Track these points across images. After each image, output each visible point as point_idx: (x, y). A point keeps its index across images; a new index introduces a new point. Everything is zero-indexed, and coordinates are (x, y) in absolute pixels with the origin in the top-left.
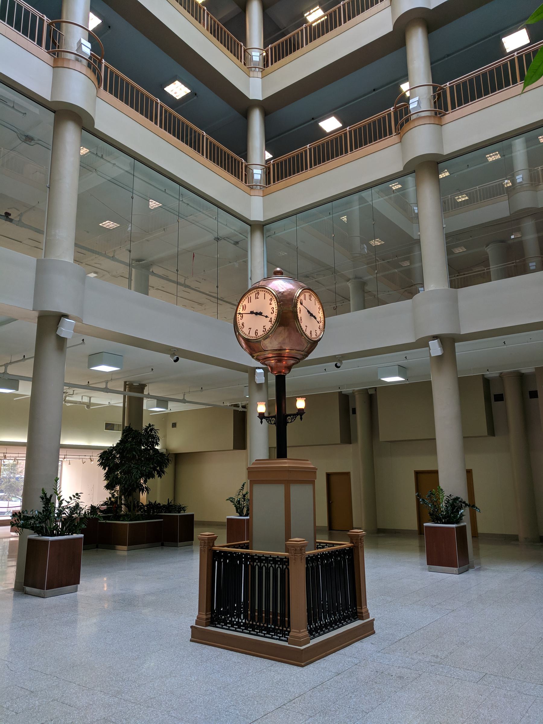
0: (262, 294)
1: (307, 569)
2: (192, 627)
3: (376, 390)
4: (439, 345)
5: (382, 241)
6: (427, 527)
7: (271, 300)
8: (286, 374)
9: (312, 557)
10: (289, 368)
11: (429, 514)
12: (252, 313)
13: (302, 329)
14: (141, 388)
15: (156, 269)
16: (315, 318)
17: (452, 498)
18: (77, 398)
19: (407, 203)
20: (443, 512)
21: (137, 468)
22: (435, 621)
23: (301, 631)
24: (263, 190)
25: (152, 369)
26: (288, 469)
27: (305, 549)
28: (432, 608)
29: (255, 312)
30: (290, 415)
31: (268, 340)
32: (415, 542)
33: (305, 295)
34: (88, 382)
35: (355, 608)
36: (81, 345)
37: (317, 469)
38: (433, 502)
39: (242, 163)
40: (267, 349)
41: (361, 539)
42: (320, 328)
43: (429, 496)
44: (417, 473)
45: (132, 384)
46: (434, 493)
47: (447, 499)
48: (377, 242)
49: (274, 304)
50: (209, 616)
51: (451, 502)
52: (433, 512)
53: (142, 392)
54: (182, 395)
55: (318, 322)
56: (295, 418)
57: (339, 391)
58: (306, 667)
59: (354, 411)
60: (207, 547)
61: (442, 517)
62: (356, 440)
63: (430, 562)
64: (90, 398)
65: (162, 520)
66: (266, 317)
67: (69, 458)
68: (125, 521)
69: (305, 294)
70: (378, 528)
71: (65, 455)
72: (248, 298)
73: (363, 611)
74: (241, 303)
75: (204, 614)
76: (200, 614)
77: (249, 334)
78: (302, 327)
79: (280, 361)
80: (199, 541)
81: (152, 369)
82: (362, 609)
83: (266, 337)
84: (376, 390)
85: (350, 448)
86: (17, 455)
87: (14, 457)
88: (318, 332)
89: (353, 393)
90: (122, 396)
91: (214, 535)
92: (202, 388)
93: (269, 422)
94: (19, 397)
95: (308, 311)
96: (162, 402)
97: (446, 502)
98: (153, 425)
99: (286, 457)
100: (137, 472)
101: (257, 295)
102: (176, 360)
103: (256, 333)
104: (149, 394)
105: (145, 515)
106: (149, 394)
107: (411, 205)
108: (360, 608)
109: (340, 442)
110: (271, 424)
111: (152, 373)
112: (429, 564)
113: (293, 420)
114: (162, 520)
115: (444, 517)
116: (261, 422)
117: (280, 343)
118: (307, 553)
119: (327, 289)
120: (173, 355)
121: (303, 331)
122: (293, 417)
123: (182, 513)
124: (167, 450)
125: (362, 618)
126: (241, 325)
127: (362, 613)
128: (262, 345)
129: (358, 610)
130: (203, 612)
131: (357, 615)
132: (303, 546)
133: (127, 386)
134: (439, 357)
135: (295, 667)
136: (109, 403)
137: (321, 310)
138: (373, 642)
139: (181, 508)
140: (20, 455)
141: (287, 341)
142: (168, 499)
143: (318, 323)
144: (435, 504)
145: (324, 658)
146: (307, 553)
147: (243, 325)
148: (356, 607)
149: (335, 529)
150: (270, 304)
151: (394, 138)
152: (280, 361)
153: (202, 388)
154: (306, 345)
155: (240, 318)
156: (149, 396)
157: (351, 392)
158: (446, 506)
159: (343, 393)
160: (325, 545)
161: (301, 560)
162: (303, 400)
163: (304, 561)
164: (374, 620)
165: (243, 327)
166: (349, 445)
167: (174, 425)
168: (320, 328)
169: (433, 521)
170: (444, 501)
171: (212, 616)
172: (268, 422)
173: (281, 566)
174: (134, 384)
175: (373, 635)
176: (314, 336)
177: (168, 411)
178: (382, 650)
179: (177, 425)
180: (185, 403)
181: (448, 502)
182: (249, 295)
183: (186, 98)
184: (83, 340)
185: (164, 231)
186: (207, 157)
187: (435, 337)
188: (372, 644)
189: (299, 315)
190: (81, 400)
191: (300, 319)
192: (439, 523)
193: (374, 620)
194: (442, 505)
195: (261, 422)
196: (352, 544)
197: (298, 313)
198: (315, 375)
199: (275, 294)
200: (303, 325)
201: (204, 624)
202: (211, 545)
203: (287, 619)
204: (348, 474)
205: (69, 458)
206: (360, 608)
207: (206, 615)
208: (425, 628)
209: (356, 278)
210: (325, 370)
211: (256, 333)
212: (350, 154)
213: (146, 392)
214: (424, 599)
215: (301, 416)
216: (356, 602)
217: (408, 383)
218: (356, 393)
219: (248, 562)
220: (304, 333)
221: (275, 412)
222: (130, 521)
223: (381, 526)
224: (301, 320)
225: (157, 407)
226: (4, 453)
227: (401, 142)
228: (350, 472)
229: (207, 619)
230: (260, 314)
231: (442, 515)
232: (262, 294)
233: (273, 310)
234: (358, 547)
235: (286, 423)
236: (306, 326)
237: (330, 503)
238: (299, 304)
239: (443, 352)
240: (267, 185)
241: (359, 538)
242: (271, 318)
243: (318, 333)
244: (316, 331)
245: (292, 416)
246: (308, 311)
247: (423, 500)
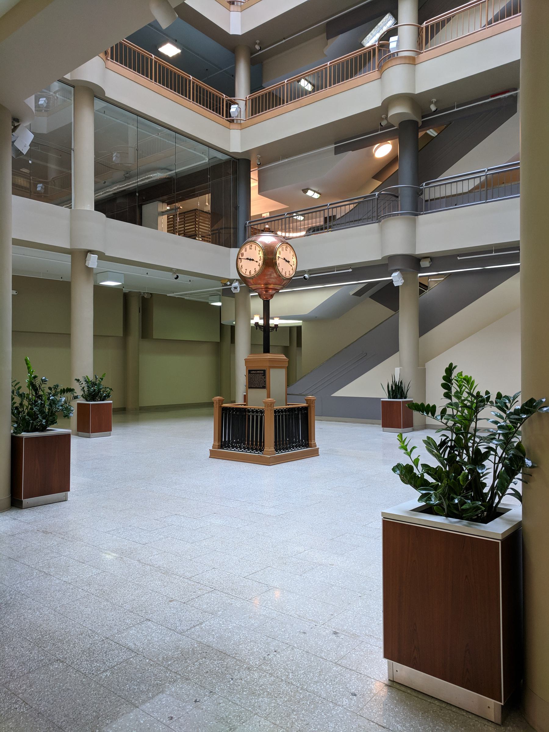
0: (254, 246)
1: (275, 416)
8: (270, 299)
10: (272, 296)
12: (247, 259)
27: (273, 405)
39: (223, 99)
49: (261, 255)
66: (257, 262)
82: (311, 442)
121: (280, 272)
126: (241, 267)
127: (311, 444)
129: (309, 443)
132: (273, 403)
135: (267, 466)
150: (259, 254)
151: (374, 74)
155: (240, 261)
176: (288, 275)
183: (178, 56)
186: (193, 100)
199: (261, 246)
200: (280, 269)
203: (262, 444)
212: (329, 89)
227: (381, 78)
229: (218, 445)
230: (253, 260)
232: (254, 246)
238: (278, 253)
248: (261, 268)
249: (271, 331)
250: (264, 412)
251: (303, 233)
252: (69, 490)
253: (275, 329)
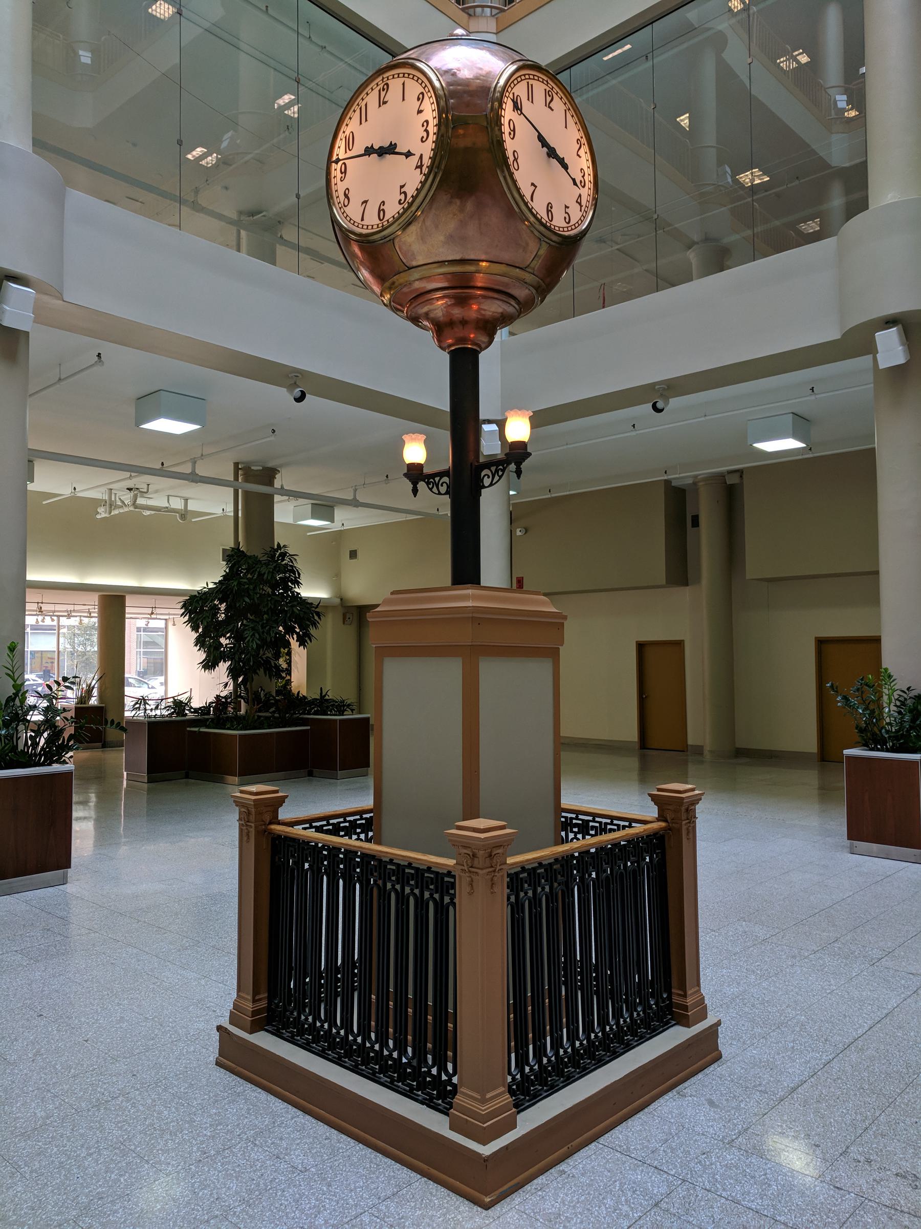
1: (516, 909)
2: (220, 1028)
3: (741, 477)
4: (901, 340)
5: (764, 174)
6: (850, 758)
7: (421, 98)
9: (534, 869)
10: (489, 327)
11: (856, 728)
12: (369, 151)
13: (518, 189)
14: (268, 475)
15: (289, 233)
16: (565, 167)
17: (912, 694)
18: (159, 501)
19: (822, 86)
20: (892, 726)
21: (253, 629)
22: (887, 1015)
23: (488, 1096)
24: (497, 18)
25: (274, 431)
26: (470, 615)
28: (871, 969)
30: (487, 465)
31: (413, 228)
32: (811, 777)
33: (530, 89)
34: (163, 464)
35: (665, 996)
36: (95, 368)
37: (565, 618)
38: (867, 702)
40: (414, 263)
41: (687, 810)
42: (580, 204)
43: (858, 690)
44: (822, 643)
45: (249, 468)
46: (871, 685)
47: (900, 696)
48: (752, 177)
49: (430, 112)
50: (264, 1004)
51: (909, 702)
52: (867, 726)
53: (271, 483)
54: (352, 490)
55: (574, 180)
56: (500, 473)
57: (666, 478)
58: (498, 1207)
59: (696, 522)
60: (253, 825)
61: (889, 737)
62: (698, 580)
63: (855, 833)
64: (186, 500)
65: (309, 728)
66: (408, 154)
67: (174, 614)
68: (234, 730)
69: (531, 82)
70: (738, 745)
71: (153, 608)
72: (358, 111)
73: (690, 1001)
74: (341, 131)
77: (362, 219)
78: (520, 184)
79: (462, 301)
80: (237, 808)
81: (274, 431)
82: (685, 996)
83: (407, 219)
84: (741, 477)
85: (684, 595)
86: (71, 608)
87: (67, 611)
88: (575, 215)
89: (695, 484)
90: (231, 490)
91: (277, 792)
92: (387, 476)
93: (435, 489)
94: (50, 499)
95: (541, 138)
96: (324, 508)
97: (898, 703)
98: (285, 546)
99: (478, 581)
100: (253, 635)
101: (383, 94)
102: (300, 399)
103: (381, 211)
104: (282, 487)
105: (275, 718)
106: (282, 487)
107: (830, 91)
109: (664, 582)
110: (440, 493)
111: (272, 438)
112: (851, 837)
113: (497, 478)
114: (309, 728)
115: (894, 736)
116: (415, 491)
117: (451, 236)
118: (510, 860)
119: (645, 270)
120: (291, 387)
121: (522, 197)
122: (497, 471)
123: (348, 716)
124: (341, 599)
125: (685, 1022)
126: (342, 197)
127: (686, 1008)
128: (400, 248)
129: (675, 999)
131: (672, 1013)
133: (240, 472)
134: (897, 371)
136: (223, 510)
137: (585, 149)
138: (714, 1098)
139: (344, 706)
140: (77, 608)
141: (471, 230)
142: (321, 689)
143: (575, 183)
144: (871, 707)
145: (563, 1166)
146: (510, 860)
147: (346, 196)
148: (669, 990)
149: (653, 747)
152: (462, 301)
153: (387, 476)
154: (533, 246)
155: (339, 175)
156: (283, 492)
157: (691, 482)
158: (900, 713)
159: (673, 484)
160: (591, 818)
161: (492, 887)
162: (523, 416)
163: (503, 890)
164: (718, 1023)
165: (346, 201)
166: (682, 588)
167: (353, 554)
168: (580, 204)
169: (864, 745)
170: (893, 701)
171: (269, 1003)
172: (431, 489)
173: (436, 896)
174: (252, 468)
175: (715, 1065)
176: (558, 222)
177: (336, 526)
178: (740, 1134)
179: (359, 554)
180: (356, 506)
181: (903, 704)
182: (363, 99)
184: (99, 355)
185: (287, 132)
187: (889, 322)
188: (711, 1103)
189: (510, 145)
190: (167, 505)
191: (511, 159)
192: (878, 750)
193: (718, 1023)
194: (890, 711)
195: (415, 491)
196: (663, 824)
197: (506, 137)
198: (614, 437)
199: (437, 84)
201: (249, 1024)
202: (267, 818)
204: (679, 644)
205: (174, 614)
207: (254, 1001)
208: (860, 1043)
209: (707, 239)
210: (634, 426)
211: (382, 213)
213: (277, 484)
214: (849, 938)
215: (518, 465)
216: (670, 978)
217: (811, 456)
218: (701, 484)
220: (526, 204)
221: (446, 462)
222: (241, 729)
223: (741, 743)
224: (516, 159)
225: (314, 516)
226: (38, 603)
228: (683, 641)
229: (254, 1013)
231: (887, 732)
234: (679, 831)
235: (477, 488)
236: (533, 184)
237: (643, 698)
238: (508, 105)
239: (909, 358)
240: (505, 6)
241: (683, 809)
242: (421, 155)
243: (575, 215)
244: (567, 207)
245: (493, 469)
246: (541, 138)
247: (845, 698)
248: (427, 176)
249: (487, 482)
250: (453, 886)
251: (511, 509)
252: (70, 867)
253: (513, 467)
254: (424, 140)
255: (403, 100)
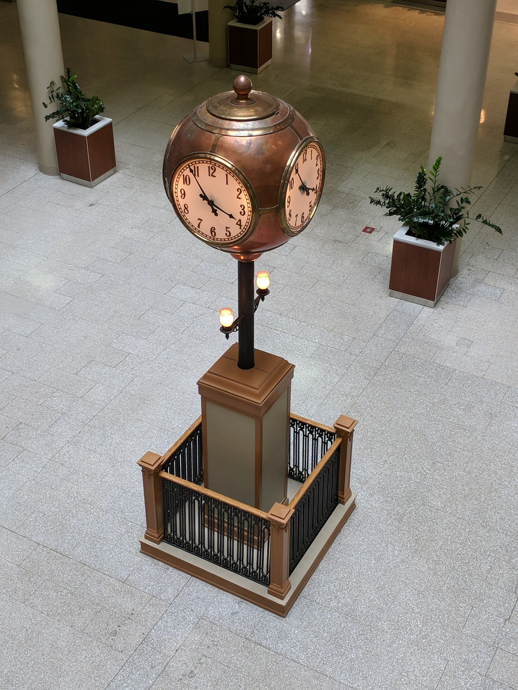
29: (206, 202)
75: (155, 532)
76: (149, 530)
101: (211, 171)
108: (342, 493)
126: (183, 208)
129: (339, 495)
130: (155, 530)
206: (342, 493)
211: (213, 233)
219: (259, 14)
233: (243, 209)
254: (242, 214)
255: (227, 184)
